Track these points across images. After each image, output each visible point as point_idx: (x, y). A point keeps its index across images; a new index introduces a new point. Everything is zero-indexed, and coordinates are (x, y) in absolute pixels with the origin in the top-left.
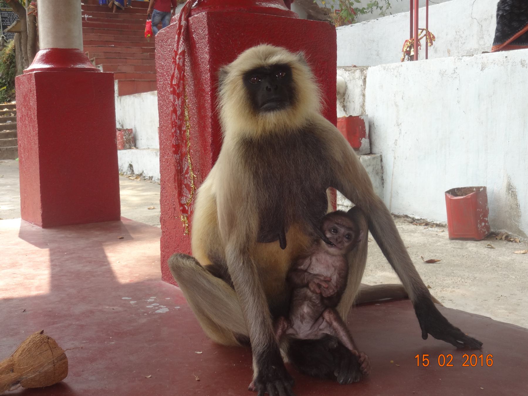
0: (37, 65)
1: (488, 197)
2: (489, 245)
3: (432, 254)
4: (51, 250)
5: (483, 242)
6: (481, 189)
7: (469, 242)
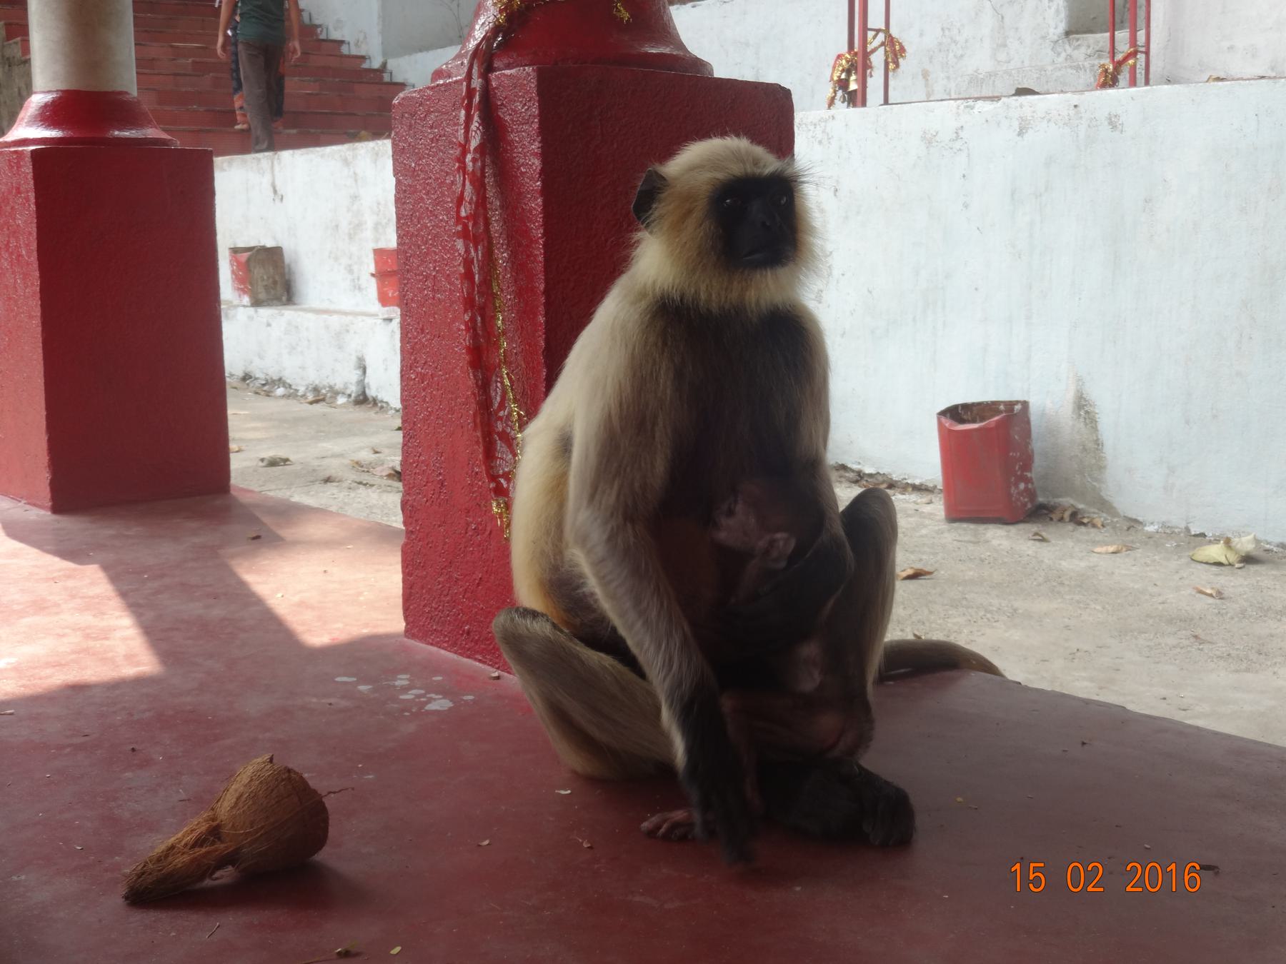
1: (1033, 424)
2: (1036, 534)
3: (912, 557)
5: (1021, 526)
6: (1018, 407)
7: (991, 526)
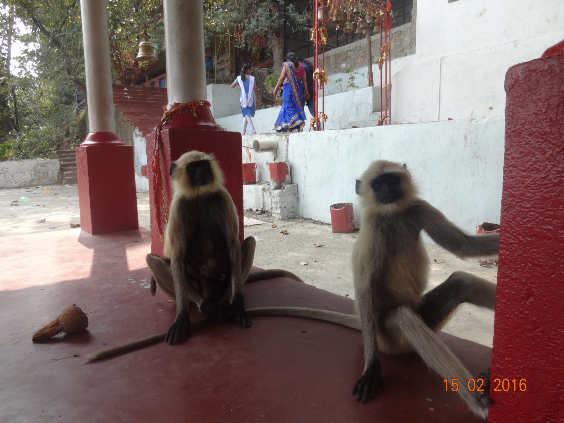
0: (88, 142)
4: (95, 250)
